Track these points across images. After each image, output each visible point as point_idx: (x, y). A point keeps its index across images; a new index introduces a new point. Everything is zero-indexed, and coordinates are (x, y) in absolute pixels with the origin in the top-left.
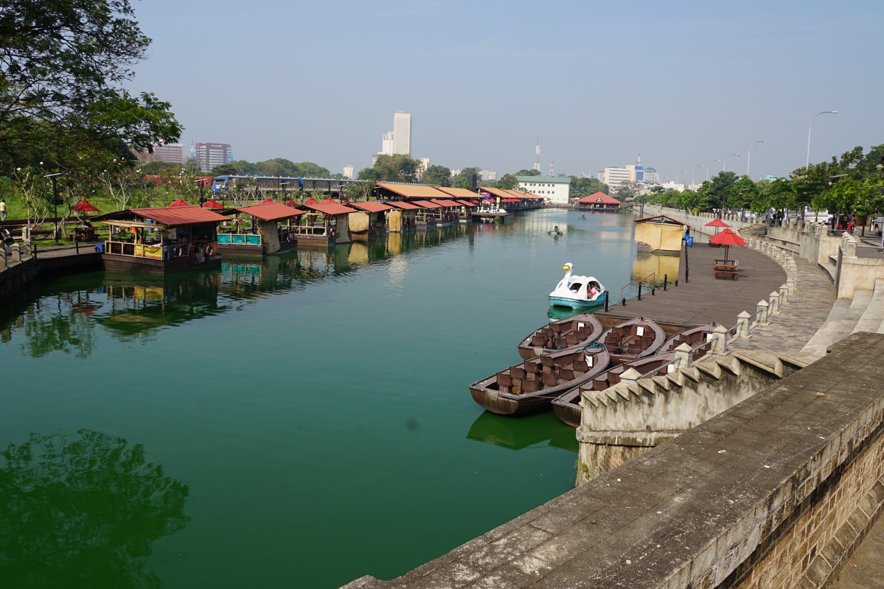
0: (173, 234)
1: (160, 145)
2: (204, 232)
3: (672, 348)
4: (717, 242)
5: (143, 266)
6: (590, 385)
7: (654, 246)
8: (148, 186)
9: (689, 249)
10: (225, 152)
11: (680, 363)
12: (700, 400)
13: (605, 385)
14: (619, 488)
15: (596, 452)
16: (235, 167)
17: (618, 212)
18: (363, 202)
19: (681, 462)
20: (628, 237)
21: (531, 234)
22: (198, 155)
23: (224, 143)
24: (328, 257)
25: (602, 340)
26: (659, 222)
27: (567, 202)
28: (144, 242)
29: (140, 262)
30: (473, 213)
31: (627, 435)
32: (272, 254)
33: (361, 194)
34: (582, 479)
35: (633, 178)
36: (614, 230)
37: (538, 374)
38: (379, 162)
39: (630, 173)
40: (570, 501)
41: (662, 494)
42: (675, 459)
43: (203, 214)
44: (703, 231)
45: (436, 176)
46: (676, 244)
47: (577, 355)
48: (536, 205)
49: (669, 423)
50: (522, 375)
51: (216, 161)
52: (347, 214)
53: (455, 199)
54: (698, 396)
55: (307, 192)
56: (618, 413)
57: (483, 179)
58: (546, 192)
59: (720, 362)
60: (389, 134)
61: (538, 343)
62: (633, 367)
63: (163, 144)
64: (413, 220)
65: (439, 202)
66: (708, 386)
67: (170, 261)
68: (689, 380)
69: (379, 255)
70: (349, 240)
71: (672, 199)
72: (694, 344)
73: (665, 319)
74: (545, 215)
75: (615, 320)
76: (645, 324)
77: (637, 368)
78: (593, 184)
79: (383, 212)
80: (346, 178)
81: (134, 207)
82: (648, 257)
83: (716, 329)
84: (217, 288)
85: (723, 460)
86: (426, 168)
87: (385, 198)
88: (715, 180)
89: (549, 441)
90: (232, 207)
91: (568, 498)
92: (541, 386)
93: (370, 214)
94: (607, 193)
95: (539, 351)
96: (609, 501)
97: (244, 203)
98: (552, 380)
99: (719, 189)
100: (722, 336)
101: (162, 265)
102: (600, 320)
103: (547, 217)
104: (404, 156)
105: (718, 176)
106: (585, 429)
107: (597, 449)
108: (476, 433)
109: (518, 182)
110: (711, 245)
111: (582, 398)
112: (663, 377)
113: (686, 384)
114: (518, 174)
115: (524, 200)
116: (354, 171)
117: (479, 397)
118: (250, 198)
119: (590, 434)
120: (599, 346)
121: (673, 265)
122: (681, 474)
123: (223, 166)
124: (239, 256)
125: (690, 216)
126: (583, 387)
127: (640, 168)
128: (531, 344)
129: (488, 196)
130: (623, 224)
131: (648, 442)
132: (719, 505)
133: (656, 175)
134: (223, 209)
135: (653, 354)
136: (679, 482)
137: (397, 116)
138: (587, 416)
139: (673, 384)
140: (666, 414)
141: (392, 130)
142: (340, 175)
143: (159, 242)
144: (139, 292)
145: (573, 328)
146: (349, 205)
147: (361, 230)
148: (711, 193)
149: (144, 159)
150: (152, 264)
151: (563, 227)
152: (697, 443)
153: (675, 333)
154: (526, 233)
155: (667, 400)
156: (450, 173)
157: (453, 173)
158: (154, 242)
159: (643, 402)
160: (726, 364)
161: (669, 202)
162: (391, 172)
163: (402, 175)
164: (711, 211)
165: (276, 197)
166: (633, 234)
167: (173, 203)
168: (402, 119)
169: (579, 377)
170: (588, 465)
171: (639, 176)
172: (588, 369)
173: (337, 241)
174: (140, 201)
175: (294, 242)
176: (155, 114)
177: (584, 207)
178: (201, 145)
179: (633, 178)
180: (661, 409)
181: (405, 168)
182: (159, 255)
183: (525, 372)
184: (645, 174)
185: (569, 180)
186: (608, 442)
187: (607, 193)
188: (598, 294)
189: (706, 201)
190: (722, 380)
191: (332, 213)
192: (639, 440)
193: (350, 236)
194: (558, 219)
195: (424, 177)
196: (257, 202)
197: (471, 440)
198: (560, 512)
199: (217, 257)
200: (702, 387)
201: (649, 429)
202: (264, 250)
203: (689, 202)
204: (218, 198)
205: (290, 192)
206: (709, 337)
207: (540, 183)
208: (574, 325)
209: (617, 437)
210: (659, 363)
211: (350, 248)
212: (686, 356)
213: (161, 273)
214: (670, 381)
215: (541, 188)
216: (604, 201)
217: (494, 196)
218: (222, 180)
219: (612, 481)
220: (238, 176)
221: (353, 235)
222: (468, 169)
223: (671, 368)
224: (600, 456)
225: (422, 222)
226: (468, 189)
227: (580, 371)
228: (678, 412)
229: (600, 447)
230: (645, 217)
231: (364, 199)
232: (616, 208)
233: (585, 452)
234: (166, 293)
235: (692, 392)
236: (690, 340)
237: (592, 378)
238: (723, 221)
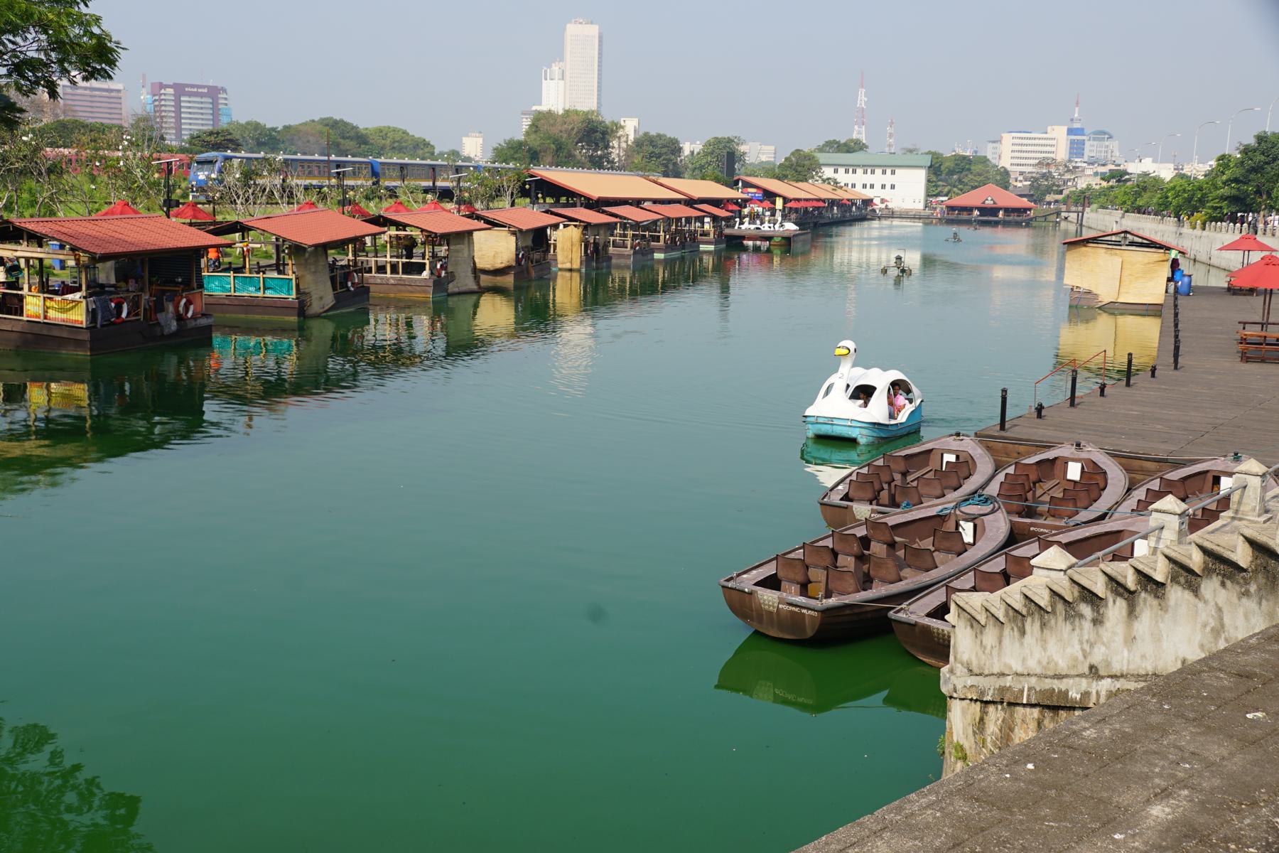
0: (106, 274)
1: (74, 83)
2: (176, 269)
3: (1143, 507)
4: (1247, 285)
5: (42, 344)
6: (968, 580)
7: (1106, 296)
8: (50, 171)
9: (1182, 301)
10: (215, 104)
11: (1160, 535)
12: (1206, 614)
13: (1001, 579)
14: (1031, 782)
15: (982, 719)
16: (237, 135)
17: (1028, 225)
18: (502, 209)
19: (1165, 733)
20: (1050, 276)
21: (844, 277)
22: (158, 109)
23: (211, 83)
24: (433, 324)
25: (993, 489)
26: (1118, 244)
27: (921, 206)
28: (44, 288)
29: (36, 330)
30: (727, 231)
31: (1048, 684)
32: (318, 316)
33: (498, 193)
34: (953, 768)
35: (1062, 154)
36: (1020, 264)
37: (861, 558)
38: (535, 127)
39: (1057, 143)
40: (929, 806)
41: (1125, 799)
42: (1152, 728)
43: (174, 233)
44: (1213, 261)
45: (652, 155)
46: (1154, 289)
47: (941, 518)
48: (856, 213)
49: (1137, 659)
50: (827, 560)
51: (196, 121)
52: (470, 233)
53: (690, 202)
54: (1201, 605)
55: (387, 188)
56: (1028, 638)
57: (748, 160)
59: (1248, 533)
60: (555, 68)
61: (861, 494)
62: (1059, 543)
63: (78, 79)
64: (606, 245)
65: (658, 208)
66: (1223, 584)
67: (103, 331)
68: (1181, 570)
69: (537, 315)
70: (475, 287)
71: (1146, 196)
72: (1192, 499)
73: (1129, 446)
74: (875, 233)
75: (1021, 449)
76: (1084, 455)
77: (1068, 547)
78: (976, 168)
79: (543, 229)
80: (468, 159)
81: (22, 215)
82: (1094, 318)
83: (1243, 467)
84: (203, 386)
85: (1257, 732)
86: (631, 138)
87: (549, 200)
88: (1246, 151)
89: (885, 693)
90: (232, 218)
91: (924, 801)
92: (866, 582)
93: (518, 233)
94: (1005, 185)
95: (862, 510)
96: (1009, 809)
97: (259, 211)
98: (890, 571)
99: (1254, 170)
100: (1255, 482)
101: (86, 336)
102: (989, 448)
103: (880, 238)
104: (587, 113)
105: (1252, 141)
106: (960, 670)
107: (984, 713)
108: (734, 677)
109: (820, 166)
110: (1232, 291)
111: (953, 607)
112: (1123, 565)
113: (1174, 579)
114: (821, 150)
115: (833, 203)
116: (484, 145)
117: (740, 604)
118: (271, 201)
119: (970, 681)
120: (986, 501)
121: (1145, 337)
122: (1165, 758)
123: (211, 133)
124: (249, 318)
125: (1186, 230)
126: (954, 584)
127: (1080, 131)
128: (846, 497)
129: (759, 195)
130: (1039, 250)
131: (1093, 698)
132: (1252, 827)
133: (1114, 145)
134: (215, 223)
135: (1102, 517)
136: (1160, 775)
137: (572, 29)
138: (963, 643)
139: (1145, 579)
140: (1131, 640)
141: (562, 60)
142: (455, 154)
143: (79, 289)
144: (36, 395)
145: (934, 464)
146: (473, 216)
147: (499, 266)
148: (1236, 180)
149: (39, 110)
150: (65, 335)
151: (913, 259)
152: (1199, 696)
153: (1150, 474)
154: (837, 270)
155: (1132, 612)
156: (680, 149)
157: (687, 148)
158: (66, 289)
159: (1081, 616)
160: (1262, 539)
161: (1140, 202)
162: (560, 147)
163: (581, 152)
164: (1233, 219)
165: (324, 198)
166: (1061, 271)
167: (106, 208)
168: (581, 37)
169: (947, 565)
170: (966, 745)
171: (1076, 148)
172: (964, 548)
173: (452, 288)
174: (33, 203)
175: (363, 291)
176: (59, 14)
177: (958, 216)
178: (162, 86)
179: (1062, 154)
180: (1121, 630)
181: (590, 139)
182: (79, 316)
183: (835, 554)
184: (1087, 144)
185: (927, 161)
186: (1008, 697)
187: (1005, 185)
188: (909, 408)
189: (1223, 198)
190: (1256, 571)
191: (440, 230)
192: (1075, 695)
193: (477, 279)
194: (904, 242)
195: (628, 156)
196: (285, 209)
197: (725, 692)
198: (908, 828)
199: (203, 322)
200: (1210, 587)
201: (1094, 672)
202: (301, 308)
203: (1186, 202)
204: (202, 199)
205: (352, 188)
206: (1226, 483)
207: (865, 167)
208: (934, 458)
209: (1027, 688)
210: (1116, 535)
211: (476, 306)
212: (1174, 522)
213: (84, 354)
214: (1138, 571)
215: (869, 179)
216: (1000, 204)
217: (770, 196)
218: (210, 162)
219: (1016, 769)
220: (243, 154)
221: (483, 277)
222: (718, 141)
223: (1141, 548)
224: (992, 727)
225: (622, 252)
226: (717, 180)
227: (948, 551)
228: (1157, 639)
229: (991, 708)
230: (1087, 234)
231: (506, 202)
232: (1024, 217)
233: (959, 719)
234: (94, 394)
235: (1188, 595)
236: (1184, 489)
237: (974, 567)
238: (1260, 238)
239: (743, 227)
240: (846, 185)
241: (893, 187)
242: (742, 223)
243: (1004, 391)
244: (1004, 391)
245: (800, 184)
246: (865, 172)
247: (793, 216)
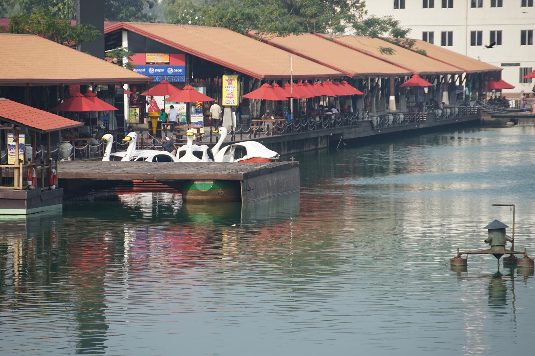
58: (511, 38)
115: (396, 85)
129: (177, 70)
217: (205, 72)
226: (56, 35)
239: (126, 156)
240: (428, 37)
242: (120, 145)
245: (291, 40)
247: (269, 123)
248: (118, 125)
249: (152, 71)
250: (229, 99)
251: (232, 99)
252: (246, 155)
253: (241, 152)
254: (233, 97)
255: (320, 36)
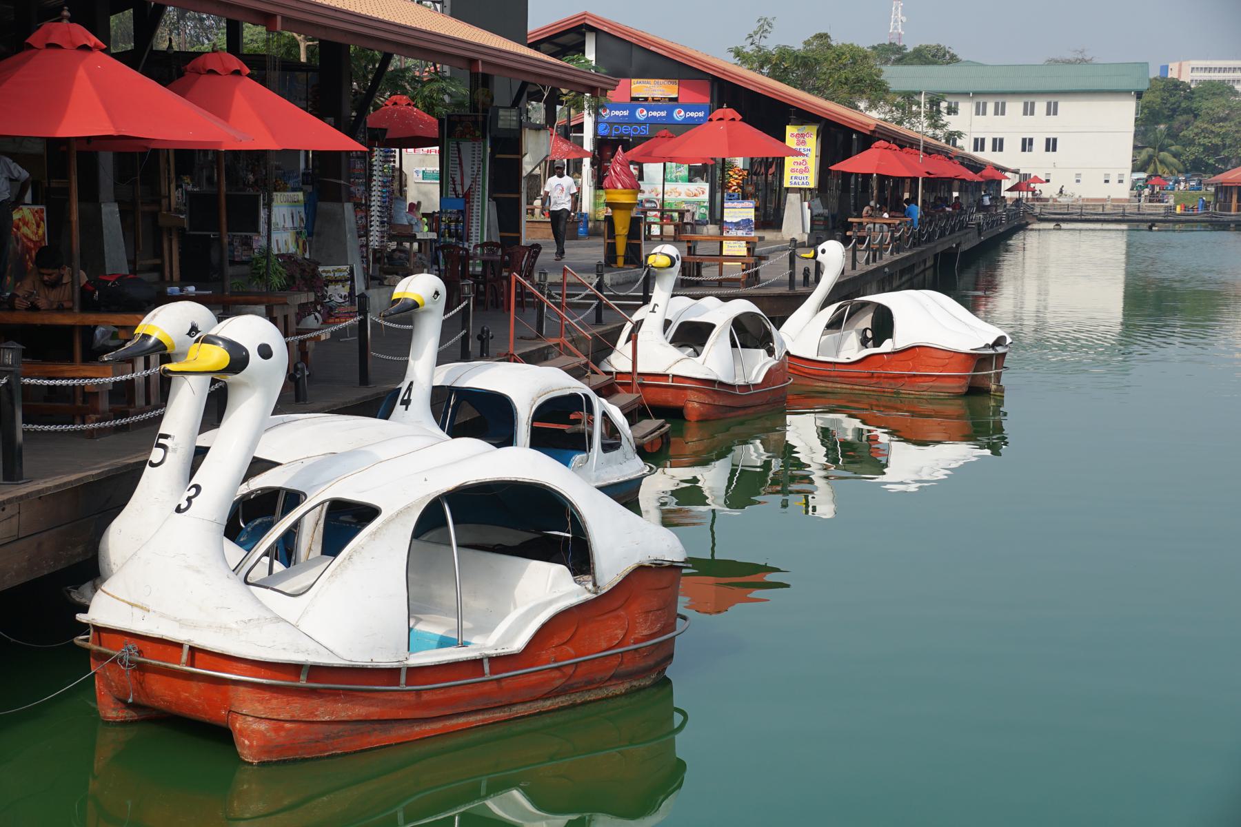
58: (1012, 145)
241: (1051, 145)
243: (788, 586)
244: (788, 586)
246: (981, 110)
248: (502, 227)
249: (641, 114)
250: (798, 175)
251: (805, 175)
252: (890, 335)
253: (884, 324)
254: (806, 170)
255: (301, 460)
